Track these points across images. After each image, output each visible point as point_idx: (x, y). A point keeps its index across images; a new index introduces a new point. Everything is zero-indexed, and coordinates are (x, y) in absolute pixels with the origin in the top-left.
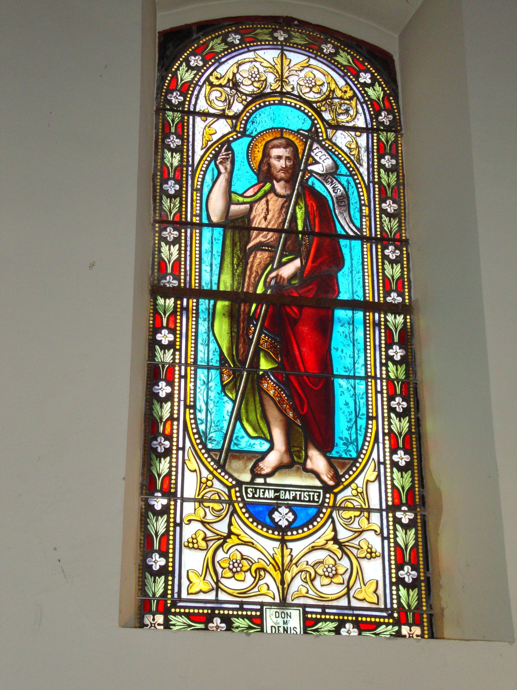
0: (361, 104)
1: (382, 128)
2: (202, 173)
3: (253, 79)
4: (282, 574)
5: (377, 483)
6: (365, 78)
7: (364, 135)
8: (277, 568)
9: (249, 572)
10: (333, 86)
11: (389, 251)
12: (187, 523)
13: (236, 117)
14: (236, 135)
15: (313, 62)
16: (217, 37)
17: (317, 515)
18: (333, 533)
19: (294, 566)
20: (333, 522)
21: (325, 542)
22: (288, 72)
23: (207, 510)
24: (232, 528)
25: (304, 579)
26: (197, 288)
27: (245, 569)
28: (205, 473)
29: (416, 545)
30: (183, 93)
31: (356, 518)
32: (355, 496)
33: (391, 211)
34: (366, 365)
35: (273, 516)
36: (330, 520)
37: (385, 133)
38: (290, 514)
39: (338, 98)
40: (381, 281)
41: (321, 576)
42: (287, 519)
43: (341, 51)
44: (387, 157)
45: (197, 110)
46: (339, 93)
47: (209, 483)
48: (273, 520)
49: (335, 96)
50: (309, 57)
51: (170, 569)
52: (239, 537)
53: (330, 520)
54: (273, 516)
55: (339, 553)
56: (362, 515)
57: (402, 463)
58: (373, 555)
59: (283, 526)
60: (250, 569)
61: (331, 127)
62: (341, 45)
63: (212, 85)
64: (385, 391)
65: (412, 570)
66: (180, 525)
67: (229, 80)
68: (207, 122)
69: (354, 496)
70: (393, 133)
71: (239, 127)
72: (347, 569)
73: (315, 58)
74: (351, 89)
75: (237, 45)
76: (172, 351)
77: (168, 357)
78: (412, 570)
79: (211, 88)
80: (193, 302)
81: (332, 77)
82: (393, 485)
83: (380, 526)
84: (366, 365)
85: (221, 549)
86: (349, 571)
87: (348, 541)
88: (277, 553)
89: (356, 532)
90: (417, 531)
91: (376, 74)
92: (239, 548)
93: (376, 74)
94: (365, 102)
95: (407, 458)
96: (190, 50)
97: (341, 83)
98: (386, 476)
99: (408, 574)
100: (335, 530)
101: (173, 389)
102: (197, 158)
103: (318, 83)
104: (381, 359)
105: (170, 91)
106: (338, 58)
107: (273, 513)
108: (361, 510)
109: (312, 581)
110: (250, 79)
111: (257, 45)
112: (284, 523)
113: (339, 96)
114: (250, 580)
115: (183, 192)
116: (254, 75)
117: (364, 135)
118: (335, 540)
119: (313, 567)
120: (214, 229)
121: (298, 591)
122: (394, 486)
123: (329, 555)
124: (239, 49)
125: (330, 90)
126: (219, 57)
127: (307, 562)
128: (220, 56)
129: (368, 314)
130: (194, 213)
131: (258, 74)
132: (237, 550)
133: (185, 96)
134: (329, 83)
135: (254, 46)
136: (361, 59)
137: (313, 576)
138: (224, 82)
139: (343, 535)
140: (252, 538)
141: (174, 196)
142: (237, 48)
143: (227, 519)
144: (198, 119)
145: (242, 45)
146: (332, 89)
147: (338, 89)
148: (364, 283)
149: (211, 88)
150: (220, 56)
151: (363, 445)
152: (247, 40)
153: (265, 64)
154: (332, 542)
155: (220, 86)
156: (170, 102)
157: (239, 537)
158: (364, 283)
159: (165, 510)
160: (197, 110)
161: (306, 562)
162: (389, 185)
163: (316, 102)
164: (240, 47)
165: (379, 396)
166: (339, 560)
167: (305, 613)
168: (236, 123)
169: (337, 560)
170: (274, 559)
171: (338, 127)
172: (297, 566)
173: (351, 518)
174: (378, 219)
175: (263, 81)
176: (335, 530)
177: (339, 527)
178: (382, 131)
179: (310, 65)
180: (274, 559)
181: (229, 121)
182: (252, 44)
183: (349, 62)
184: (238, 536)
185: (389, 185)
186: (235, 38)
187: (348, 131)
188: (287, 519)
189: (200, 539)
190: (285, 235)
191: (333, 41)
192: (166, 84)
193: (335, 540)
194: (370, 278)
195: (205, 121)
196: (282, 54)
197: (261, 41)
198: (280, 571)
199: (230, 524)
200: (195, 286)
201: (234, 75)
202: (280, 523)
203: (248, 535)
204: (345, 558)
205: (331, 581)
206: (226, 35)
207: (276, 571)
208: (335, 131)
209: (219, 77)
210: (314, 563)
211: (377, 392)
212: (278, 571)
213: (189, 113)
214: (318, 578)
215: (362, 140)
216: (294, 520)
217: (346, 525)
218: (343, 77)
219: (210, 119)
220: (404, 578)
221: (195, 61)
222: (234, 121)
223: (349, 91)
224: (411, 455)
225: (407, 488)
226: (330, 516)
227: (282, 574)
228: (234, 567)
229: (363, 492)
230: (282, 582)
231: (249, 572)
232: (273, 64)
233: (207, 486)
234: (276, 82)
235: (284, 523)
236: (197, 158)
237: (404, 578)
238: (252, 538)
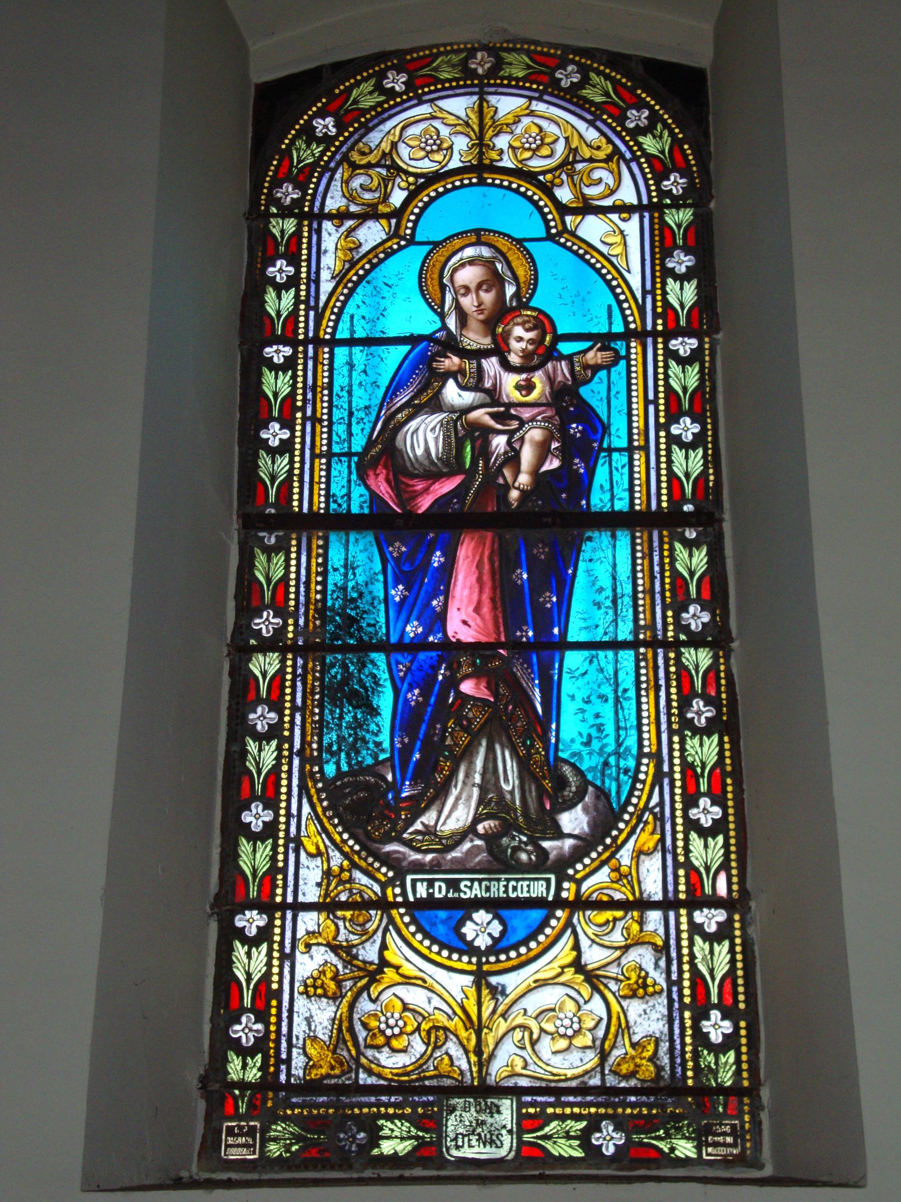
0: (627, 163)
1: (668, 201)
2: (333, 317)
3: (428, 148)
4: (478, 1034)
5: (658, 856)
6: (636, 118)
7: (636, 218)
8: (468, 1025)
9: (417, 1034)
10: (575, 143)
11: (670, 183)
12: (304, 950)
13: (398, 213)
14: (398, 244)
15: (539, 107)
16: (365, 80)
17: (545, 923)
18: (574, 953)
19: (501, 1019)
20: (575, 933)
21: (560, 970)
22: (492, 129)
23: (341, 923)
24: (386, 953)
25: (519, 1041)
26: (322, 511)
27: (409, 1029)
28: (337, 859)
29: (731, 973)
30: (302, 186)
31: (618, 923)
32: (616, 882)
33: (697, 703)
34: (631, 490)
35: (464, 930)
36: (569, 931)
37: (692, 651)
38: (496, 923)
39: (584, 160)
40: (664, 485)
41: (551, 1034)
42: (490, 935)
43: (593, 75)
44: (692, 609)
45: (327, 210)
46: (586, 153)
47: (345, 875)
48: (462, 937)
49: (578, 158)
50: (530, 99)
51: (275, 986)
52: (400, 971)
53: (569, 931)
54: (464, 930)
55: (586, 990)
56: (629, 916)
57: (688, 437)
58: (651, 989)
59: (483, 948)
60: (418, 1029)
61: (574, 211)
62: (593, 63)
63: (354, 166)
64: (662, 401)
65: (712, 805)
66: (292, 957)
67: (384, 155)
68: (343, 229)
69: (612, 882)
70: (688, 210)
71: (404, 227)
72: (601, 1019)
73: (540, 99)
74: (609, 141)
75: (400, 95)
76: (274, 743)
77: (257, 961)
78: (712, 805)
79: (353, 172)
80: (321, 464)
81: (573, 127)
82: (667, 385)
83: (663, 937)
84: (631, 490)
85: (365, 995)
86: (604, 1022)
87: (599, 969)
88: (469, 995)
89: (616, 948)
90: (727, 839)
91: (657, 107)
92: (399, 990)
93: (657, 107)
94: (635, 158)
95: (696, 428)
96: (314, 109)
97: (591, 135)
98: (658, 450)
99: (717, 1027)
100: (577, 947)
101: (277, 815)
102: (323, 298)
103: (547, 140)
104: (657, 417)
105: (277, 183)
106: (587, 92)
107: (464, 925)
108: (624, 905)
109: (533, 1043)
110: (423, 149)
111: (437, 90)
112: (483, 942)
113: (587, 156)
114: (418, 1047)
115: (295, 478)
116: (430, 142)
117: (636, 218)
118: (577, 965)
119: (536, 1018)
120: (352, 536)
121: (507, 1066)
122: (671, 474)
123: (567, 994)
124: (403, 102)
125: (570, 149)
126: (366, 119)
127: (525, 1010)
128: (368, 116)
129: (638, 534)
130: (318, 451)
131: (438, 139)
132: (394, 994)
133: (303, 187)
134: (567, 139)
135: (430, 92)
136: (629, 84)
137: (535, 1036)
138: (373, 158)
139: (593, 956)
140: (421, 970)
141: (286, 286)
142: (398, 100)
143: (378, 937)
144: (327, 225)
145: (407, 95)
146: (573, 146)
147: (584, 146)
148: (630, 409)
149: (353, 172)
150: (368, 116)
151: (630, 794)
152: (417, 82)
153: (451, 120)
154: (573, 969)
155: (369, 166)
156: (277, 202)
157: (400, 971)
158: (630, 409)
159: (265, 934)
160: (327, 210)
161: (522, 1011)
162: (687, 475)
163: (544, 173)
164: (405, 97)
165: (651, 408)
166: (586, 1002)
167: (520, 1105)
168: (398, 225)
169: (581, 1001)
170: (463, 1008)
171: (586, 208)
172: (506, 1020)
173: (608, 922)
174: (661, 370)
175: (447, 149)
176: (577, 947)
177: (584, 942)
178: (668, 207)
179: (532, 111)
180: (463, 1008)
181: (384, 222)
182: (426, 90)
183: (607, 94)
184: (397, 968)
185: (687, 475)
186: (397, 82)
187: (604, 214)
188: (490, 935)
189: (329, 975)
190: (486, 173)
191: (577, 58)
192: (271, 173)
193: (577, 965)
194: (653, 728)
195: (339, 227)
196: (482, 100)
197: (443, 82)
198: (475, 1031)
199: (384, 947)
200: (319, 508)
201: (394, 145)
202: (476, 944)
203: (413, 965)
204: (597, 997)
205: (571, 1043)
206: (382, 75)
207: (467, 1030)
208: (580, 218)
209: (367, 151)
210: (537, 1012)
211: (647, 402)
212: (471, 1030)
213: (311, 216)
214: (546, 1040)
215: (632, 227)
216: (503, 933)
217: (597, 935)
218: (591, 123)
219: (349, 223)
220: (699, 819)
221: (326, 125)
222: (393, 221)
223: (604, 146)
224: (725, 808)
225: (704, 668)
226: (569, 924)
227: (478, 1034)
228: (388, 1026)
229: (630, 873)
230: (478, 1052)
231: (417, 1034)
232: (466, 119)
233: (341, 880)
234: (471, 149)
235: (483, 942)
236: (323, 298)
237: (699, 819)
238: (421, 970)
